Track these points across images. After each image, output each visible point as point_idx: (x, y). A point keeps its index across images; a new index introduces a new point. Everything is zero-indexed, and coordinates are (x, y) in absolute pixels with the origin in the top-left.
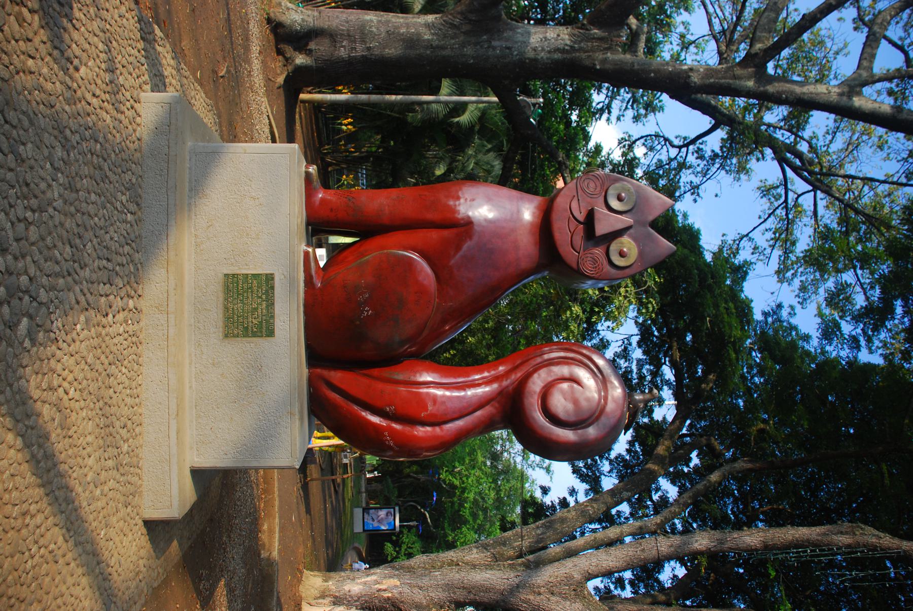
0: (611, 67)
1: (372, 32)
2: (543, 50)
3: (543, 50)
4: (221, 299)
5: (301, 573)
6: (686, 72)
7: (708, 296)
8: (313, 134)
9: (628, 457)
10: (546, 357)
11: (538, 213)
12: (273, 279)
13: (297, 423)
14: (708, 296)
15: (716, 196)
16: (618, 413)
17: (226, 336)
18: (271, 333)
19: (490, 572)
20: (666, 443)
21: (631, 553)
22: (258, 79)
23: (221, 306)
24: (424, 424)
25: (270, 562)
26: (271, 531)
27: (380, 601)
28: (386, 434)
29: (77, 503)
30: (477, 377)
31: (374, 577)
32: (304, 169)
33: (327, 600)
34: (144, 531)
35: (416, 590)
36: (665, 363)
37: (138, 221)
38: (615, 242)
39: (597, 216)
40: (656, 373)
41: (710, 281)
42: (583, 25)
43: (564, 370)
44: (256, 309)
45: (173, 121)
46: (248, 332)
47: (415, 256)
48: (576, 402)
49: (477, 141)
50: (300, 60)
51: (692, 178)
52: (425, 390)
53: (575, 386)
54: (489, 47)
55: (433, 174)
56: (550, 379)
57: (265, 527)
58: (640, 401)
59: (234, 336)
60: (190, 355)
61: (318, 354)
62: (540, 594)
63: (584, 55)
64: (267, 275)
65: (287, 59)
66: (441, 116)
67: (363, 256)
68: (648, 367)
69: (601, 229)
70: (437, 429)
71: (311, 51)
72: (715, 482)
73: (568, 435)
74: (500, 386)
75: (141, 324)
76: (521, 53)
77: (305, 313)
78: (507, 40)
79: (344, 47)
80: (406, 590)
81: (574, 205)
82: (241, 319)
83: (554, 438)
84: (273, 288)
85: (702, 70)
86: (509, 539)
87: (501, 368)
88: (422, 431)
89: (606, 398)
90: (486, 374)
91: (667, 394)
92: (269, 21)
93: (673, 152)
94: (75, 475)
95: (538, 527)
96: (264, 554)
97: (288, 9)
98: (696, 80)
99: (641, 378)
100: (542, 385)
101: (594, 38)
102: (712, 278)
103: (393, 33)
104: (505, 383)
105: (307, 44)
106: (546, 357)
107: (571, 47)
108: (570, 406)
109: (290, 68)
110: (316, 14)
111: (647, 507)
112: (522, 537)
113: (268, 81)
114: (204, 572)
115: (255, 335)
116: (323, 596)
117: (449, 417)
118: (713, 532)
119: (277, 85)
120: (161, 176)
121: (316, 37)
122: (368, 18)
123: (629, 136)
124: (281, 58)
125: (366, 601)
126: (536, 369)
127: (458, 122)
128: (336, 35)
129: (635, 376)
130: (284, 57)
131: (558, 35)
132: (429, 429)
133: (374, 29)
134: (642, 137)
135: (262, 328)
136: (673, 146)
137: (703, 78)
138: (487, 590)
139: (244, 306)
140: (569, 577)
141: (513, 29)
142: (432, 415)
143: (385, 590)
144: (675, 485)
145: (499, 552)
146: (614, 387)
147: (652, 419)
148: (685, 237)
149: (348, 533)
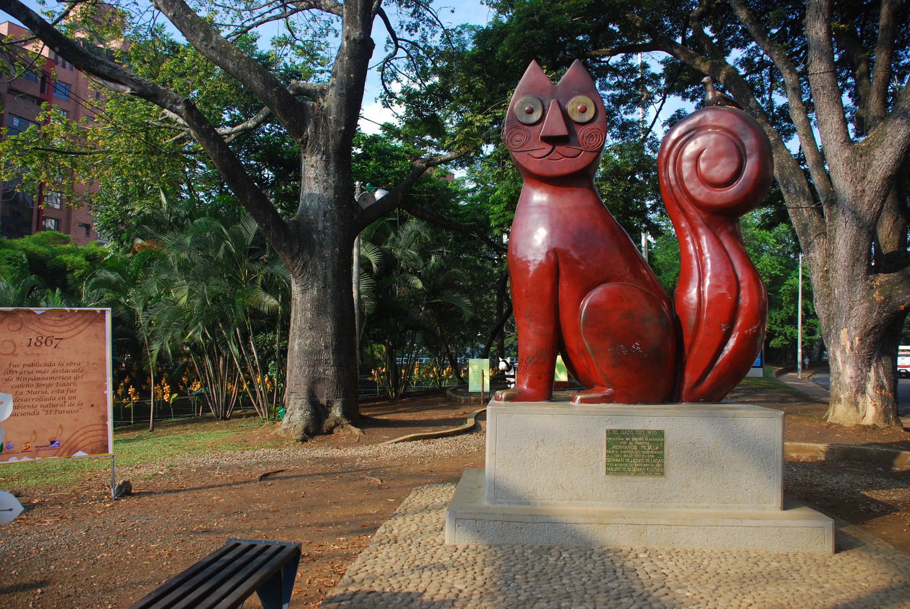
0: (344, 115)
1: (310, 344)
2: (326, 181)
3: (326, 181)
4: (629, 478)
5: (831, 424)
6: (349, 43)
7: (552, 20)
8: (369, 406)
9: (700, 100)
10: (673, 183)
11: (542, 188)
12: (611, 431)
13: (741, 411)
14: (552, 20)
15: (453, 11)
16: (730, 116)
17: (662, 474)
18: (661, 433)
19: (837, 240)
20: (698, 62)
21: (826, 100)
22: (365, 451)
23: (635, 478)
24: (737, 298)
25: (830, 452)
26: (798, 450)
27: (863, 348)
28: (746, 332)
29: (846, 602)
30: (692, 248)
31: (838, 353)
32: (503, 402)
33: (860, 399)
34: (844, 553)
35: (853, 313)
36: (607, 62)
37: (564, 548)
38: (572, 116)
39: (549, 134)
40: (615, 71)
41: (536, 18)
42: (302, 142)
43: (686, 167)
44: (639, 446)
45: (472, 516)
46: (660, 455)
47: (585, 304)
48: (719, 156)
49: (388, 246)
50: (336, 412)
51: (438, 37)
52: (706, 295)
53: (703, 156)
54: (324, 233)
55: (421, 290)
56: (696, 179)
57: (794, 455)
58: (714, 94)
59: (663, 467)
60: (679, 507)
61: (669, 392)
62: (863, 191)
63: (332, 142)
64: (607, 436)
65: (337, 425)
66: (372, 281)
67: (584, 349)
68: (607, 79)
69: (560, 129)
70: (742, 285)
71: (328, 402)
72: (747, 14)
73: (750, 165)
74: (701, 226)
75: (657, 548)
76: (330, 202)
77: (635, 403)
78: (317, 215)
79: (324, 371)
80: (853, 322)
81: (537, 154)
82: (647, 460)
83: (754, 176)
84: (619, 431)
85: (348, 28)
86: (799, 220)
87: (683, 225)
88: (745, 300)
89: (715, 127)
90: (689, 239)
91: (637, 60)
92: (304, 440)
93: (401, 53)
94: (821, 601)
95: (788, 192)
96: (822, 457)
97: (289, 422)
98: (358, 33)
99: (619, 85)
100: (702, 187)
101: (315, 132)
102: (533, 16)
103: (312, 324)
104: (699, 221)
105: (322, 405)
106: (673, 183)
107: (323, 154)
108: (723, 161)
109: (345, 422)
110: (293, 396)
111: (752, 80)
112: (798, 208)
113: (359, 442)
114: (862, 508)
115: (662, 448)
116: (856, 404)
117: (732, 273)
118: (808, 17)
119: (362, 434)
120: (521, 528)
121: (315, 396)
122: (296, 348)
123: (381, 97)
124: (335, 430)
125: (863, 362)
126: (687, 192)
127: (377, 265)
128: (314, 377)
129: (617, 92)
130: (334, 427)
131: (312, 166)
132: (742, 293)
133: (308, 342)
134: (384, 85)
135: (656, 442)
136: (395, 53)
137: (356, 27)
138: (857, 243)
139: (634, 456)
140: (848, 161)
141: (306, 209)
142: (729, 289)
143: (852, 343)
144: (730, 52)
145: (814, 231)
146: (704, 119)
147: (661, 75)
148: (489, 43)
149: (764, 383)
